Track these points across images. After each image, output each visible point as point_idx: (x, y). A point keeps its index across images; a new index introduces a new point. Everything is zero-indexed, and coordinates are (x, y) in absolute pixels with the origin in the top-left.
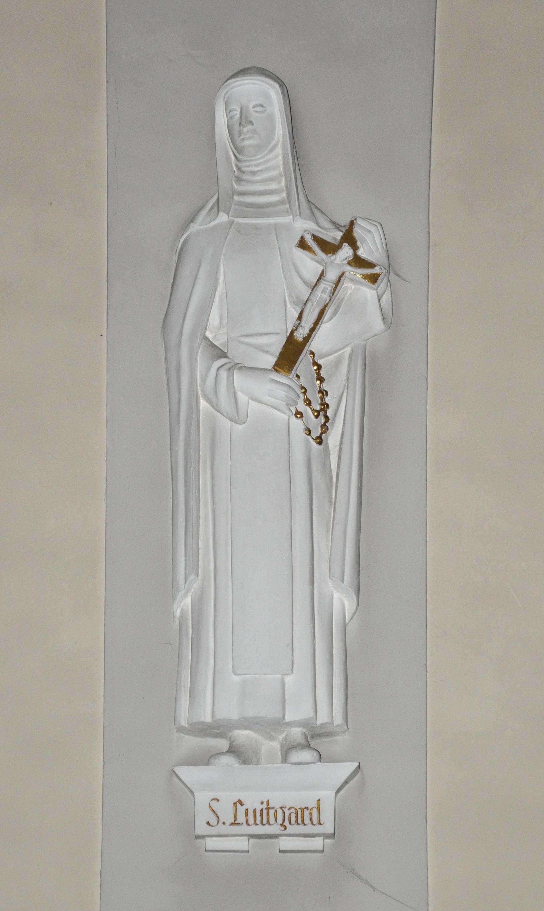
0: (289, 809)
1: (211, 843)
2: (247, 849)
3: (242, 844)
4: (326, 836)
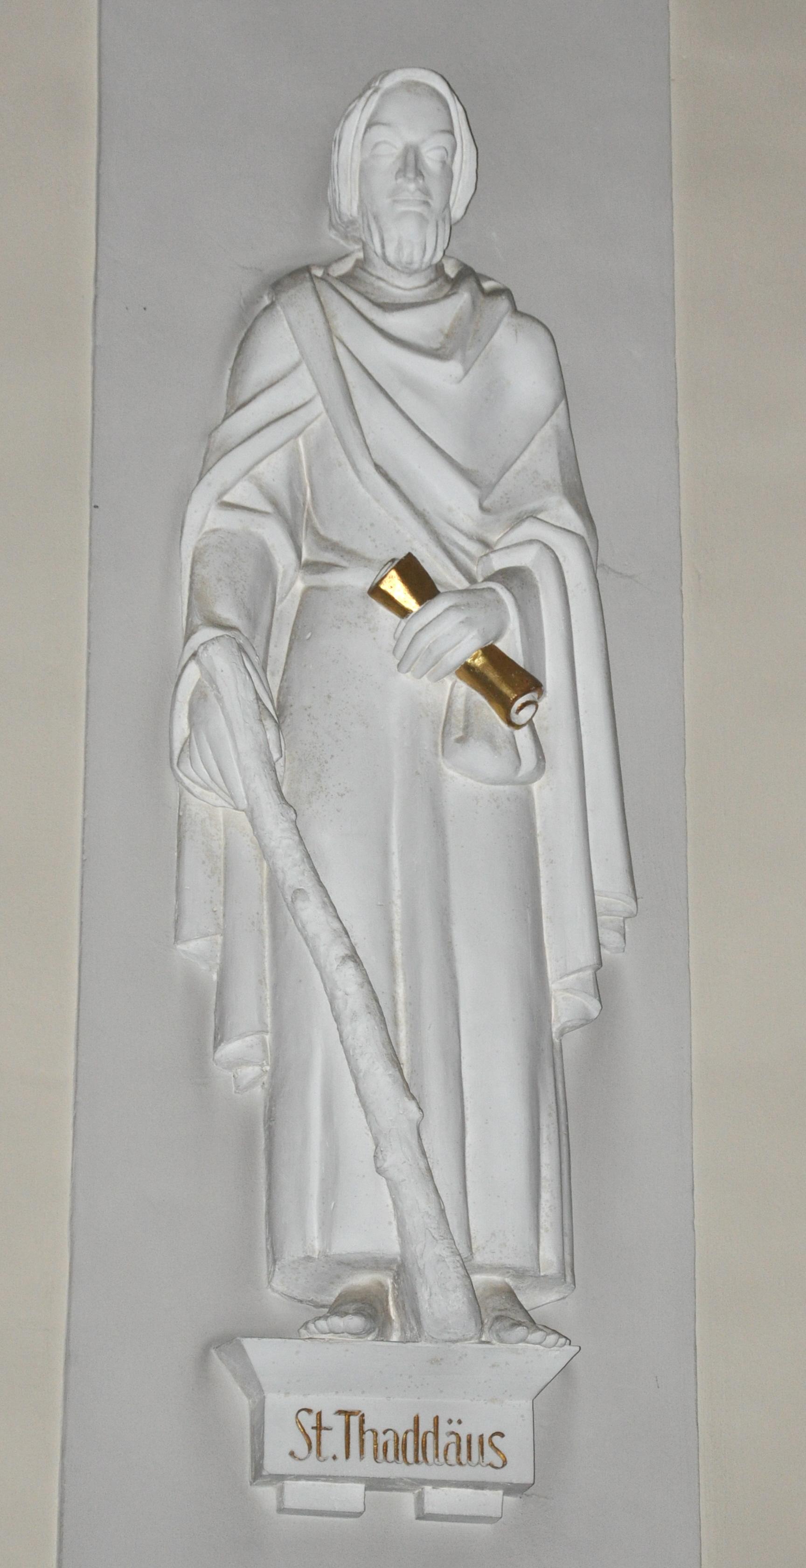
0: (385, 1433)
1: (299, 1493)
2: (360, 1508)
3: (352, 1495)
4: (510, 1489)
